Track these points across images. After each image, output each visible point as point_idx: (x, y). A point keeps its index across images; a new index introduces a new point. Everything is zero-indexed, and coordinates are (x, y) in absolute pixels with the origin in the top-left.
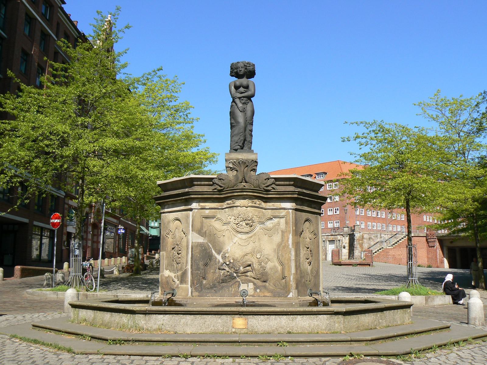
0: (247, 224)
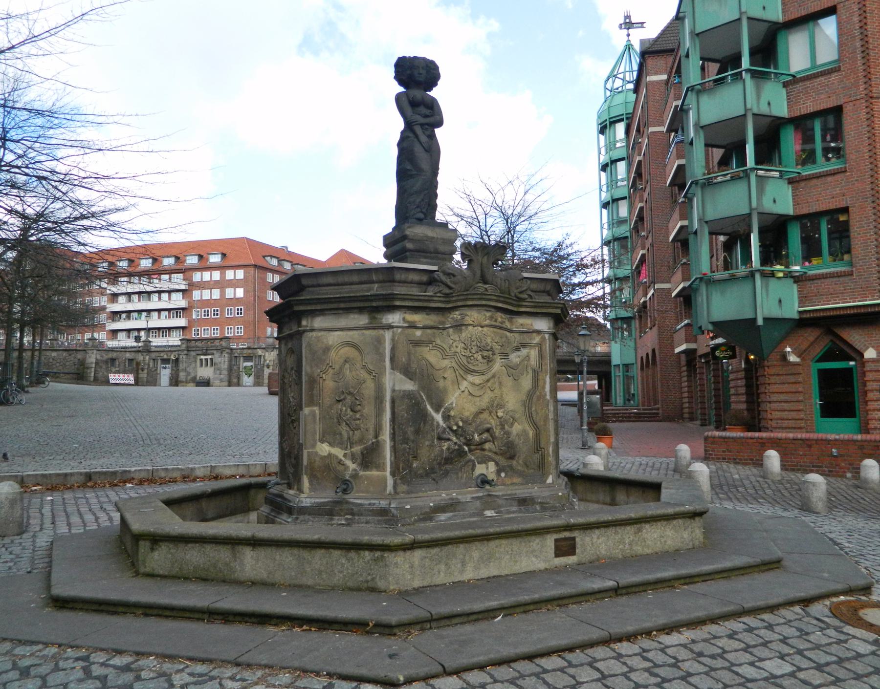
0: (483, 357)
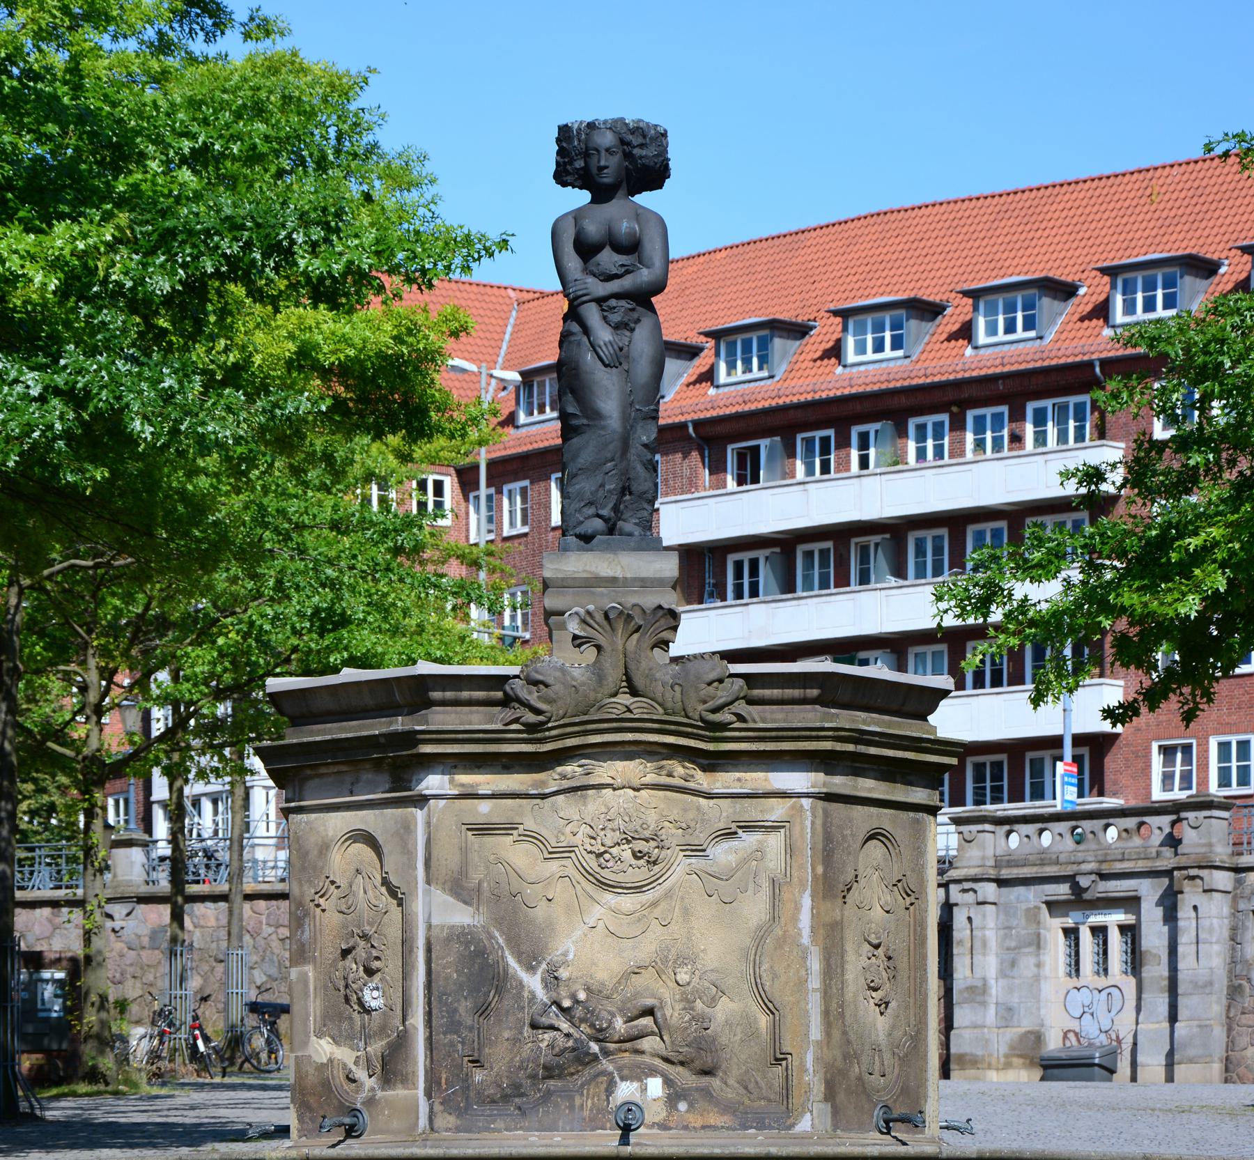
0: (637, 855)
